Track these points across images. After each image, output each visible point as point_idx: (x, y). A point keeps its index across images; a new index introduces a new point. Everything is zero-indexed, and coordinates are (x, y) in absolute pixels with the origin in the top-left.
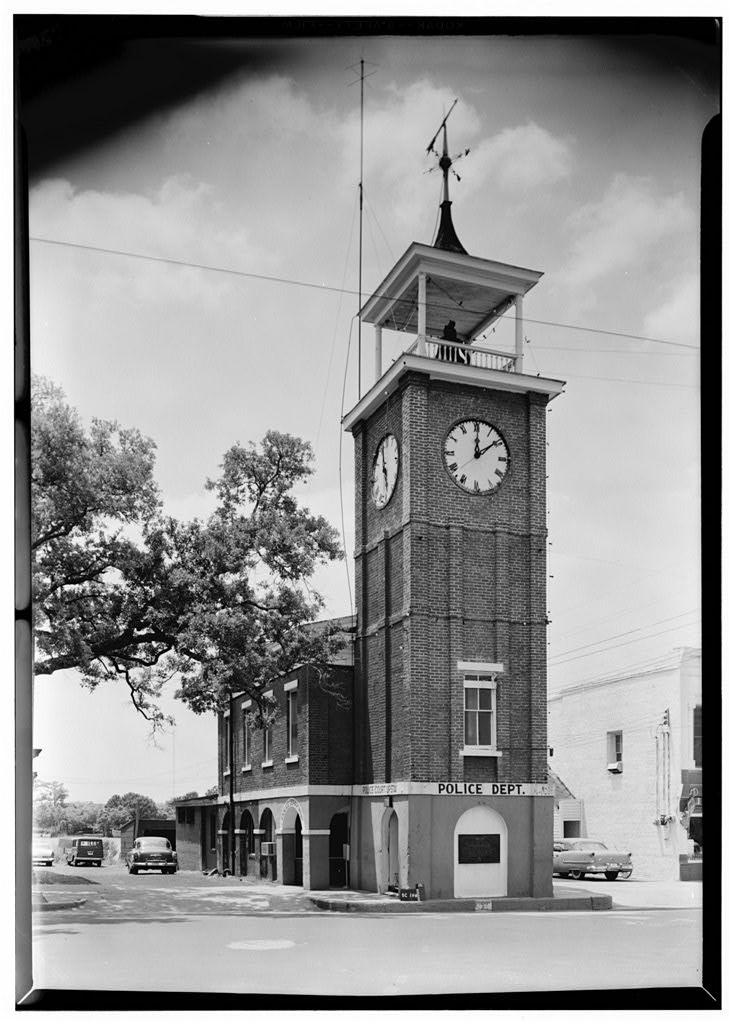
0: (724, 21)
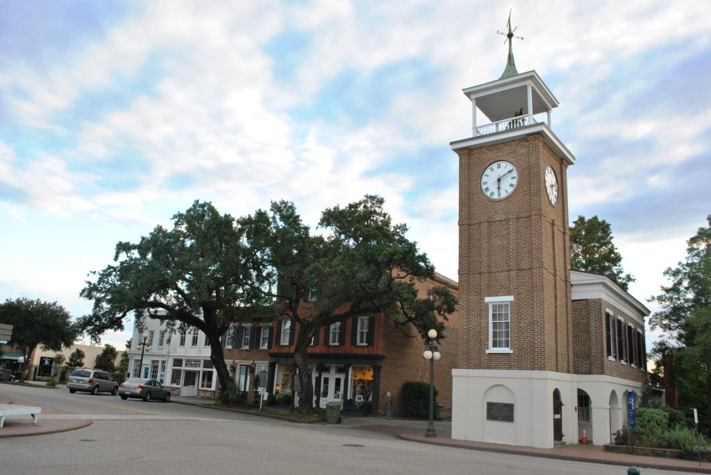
0: (536, 71)
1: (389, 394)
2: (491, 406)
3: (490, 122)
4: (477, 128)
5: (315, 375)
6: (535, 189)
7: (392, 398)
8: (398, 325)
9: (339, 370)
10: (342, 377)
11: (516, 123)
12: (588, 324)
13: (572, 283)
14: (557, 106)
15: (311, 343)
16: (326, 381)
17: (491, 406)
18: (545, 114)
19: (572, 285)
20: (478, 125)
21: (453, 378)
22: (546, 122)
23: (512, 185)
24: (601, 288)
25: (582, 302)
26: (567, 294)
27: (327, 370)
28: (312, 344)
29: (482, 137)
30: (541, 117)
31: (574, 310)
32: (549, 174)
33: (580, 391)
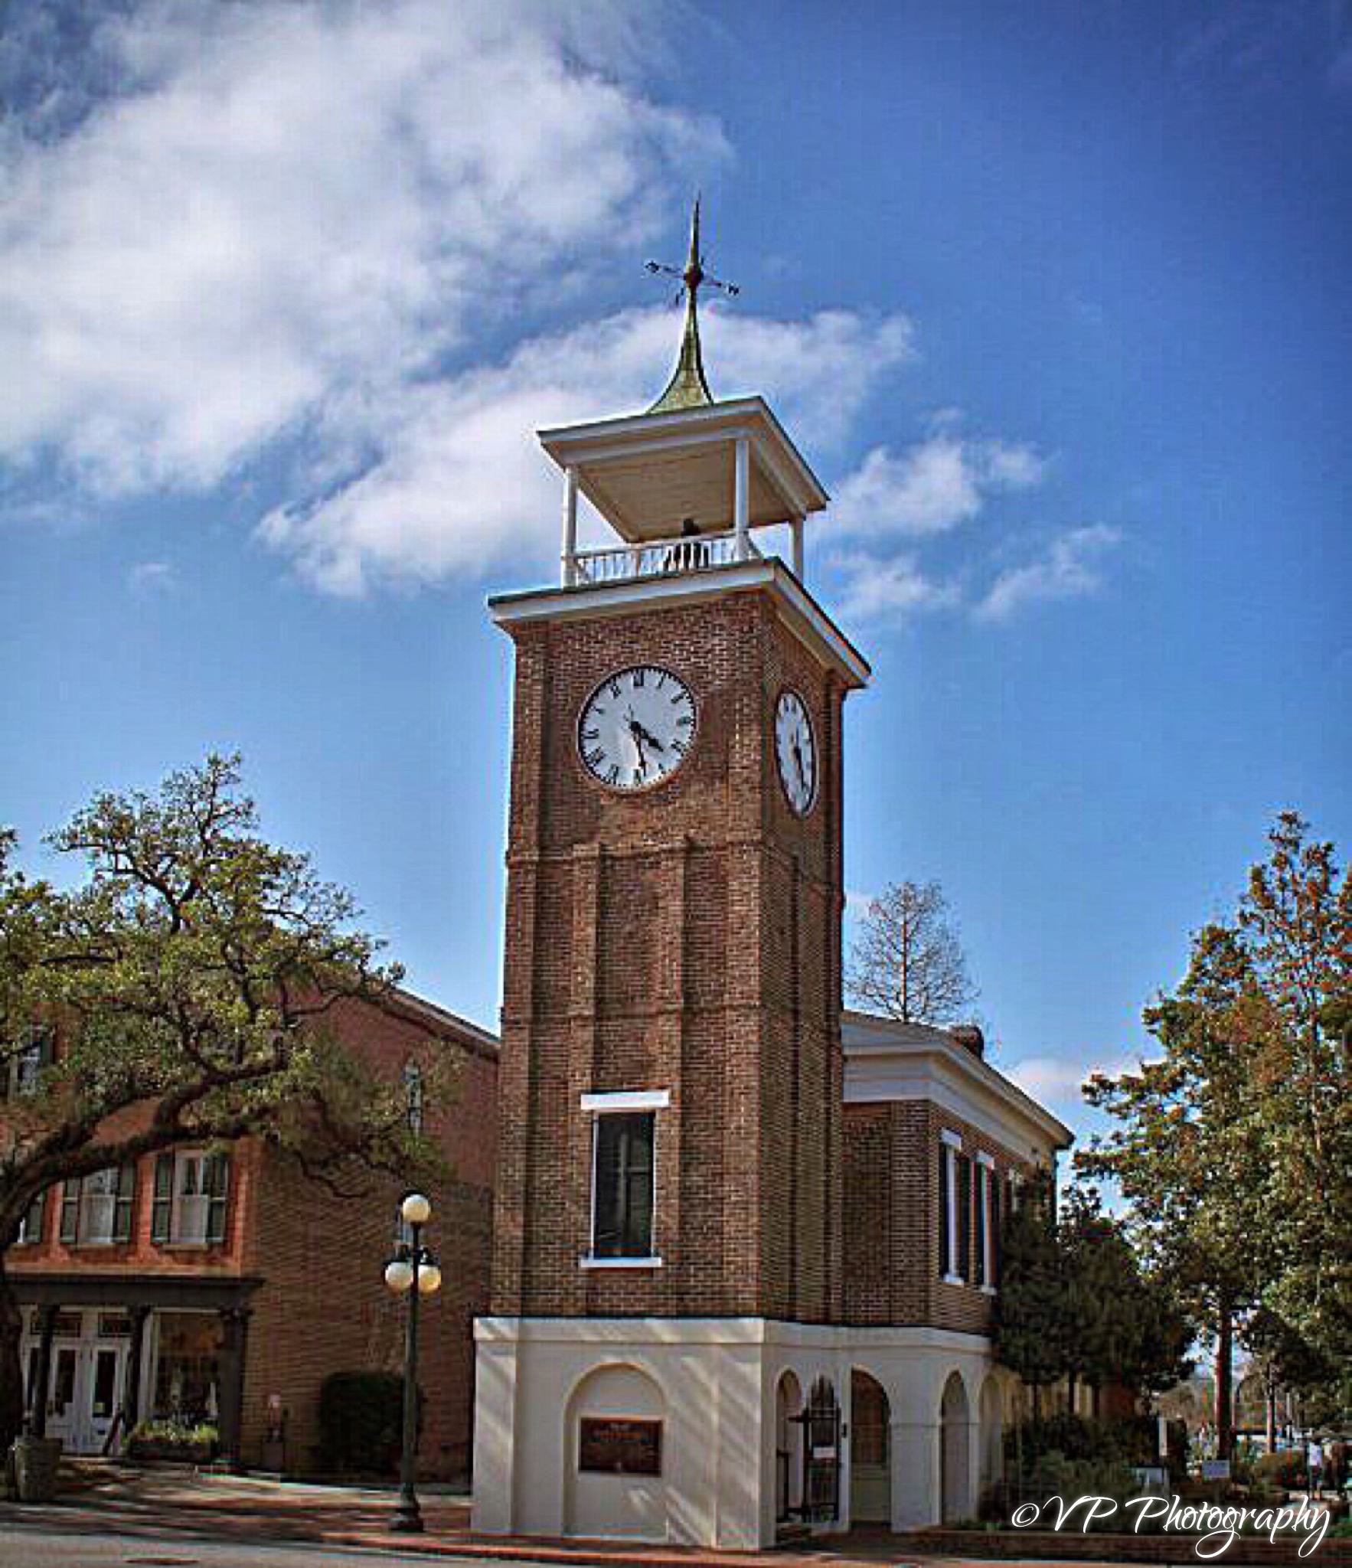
1: (275, 1401)
2: (651, 1467)
3: (622, 544)
4: (576, 558)
5: (30, 1343)
6: (745, 762)
7: (286, 1413)
8: (310, 1168)
9: (111, 1328)
10: (122, 1348)
11: (697, 558)
12: (886, 1176)
13: (847, 1052)
14: (823, 507)
15: (15, 1238)
16: (68, 1361)
17: (651, 1467)
18: (786, 530)
19: (845, 1059)
20: (579, 549)
21: (894, 1432)
22: (789, 562)
23: (683, 722)
24: (933, 1068)
25: (868, 1110)
26: (830, 1089)
27: (72, 1326)
28: (21, 1241)
29: (605, 586)
30: (773, 540)
31: (849, 1135)
32: (790, 714)
33: (956, 1374)
